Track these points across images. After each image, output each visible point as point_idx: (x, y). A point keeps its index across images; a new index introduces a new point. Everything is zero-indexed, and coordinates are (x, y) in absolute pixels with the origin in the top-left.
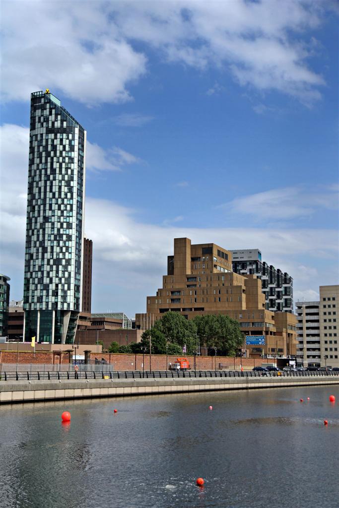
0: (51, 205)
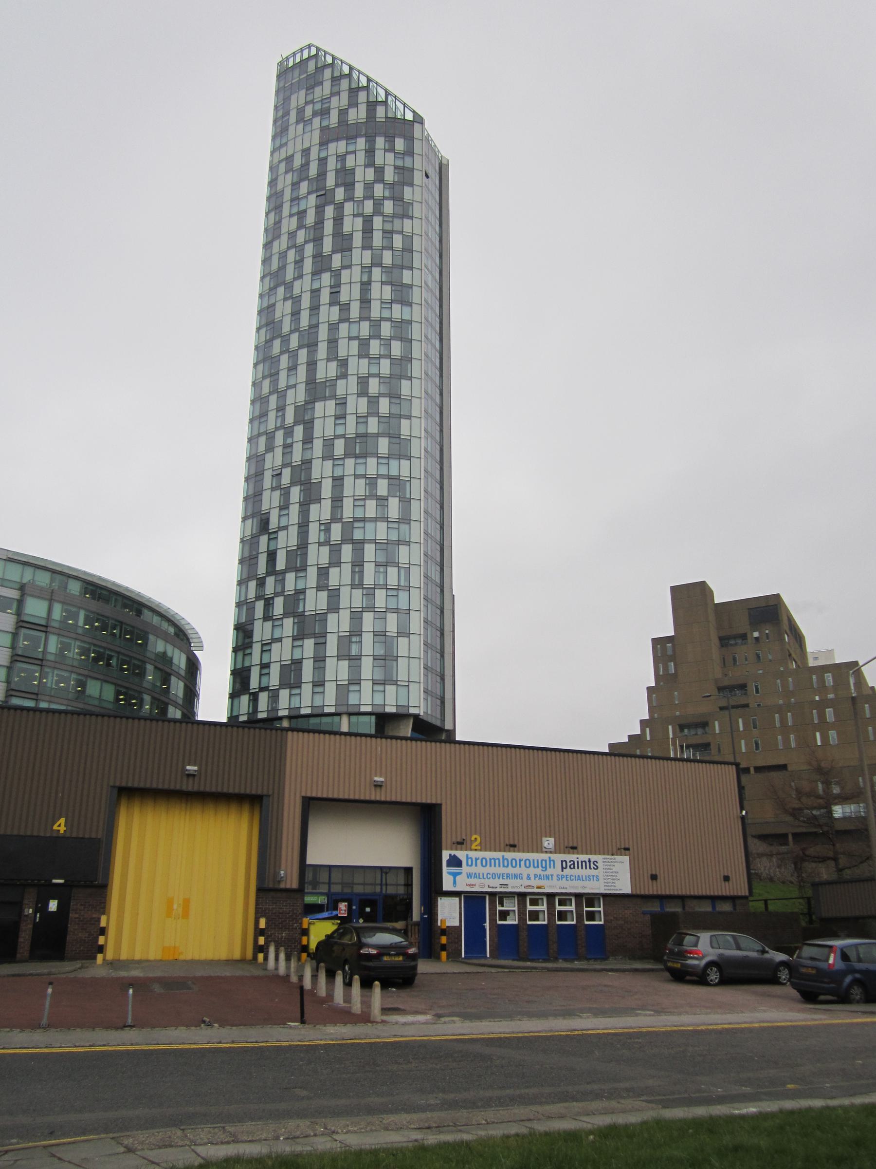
0: (333, 342)
